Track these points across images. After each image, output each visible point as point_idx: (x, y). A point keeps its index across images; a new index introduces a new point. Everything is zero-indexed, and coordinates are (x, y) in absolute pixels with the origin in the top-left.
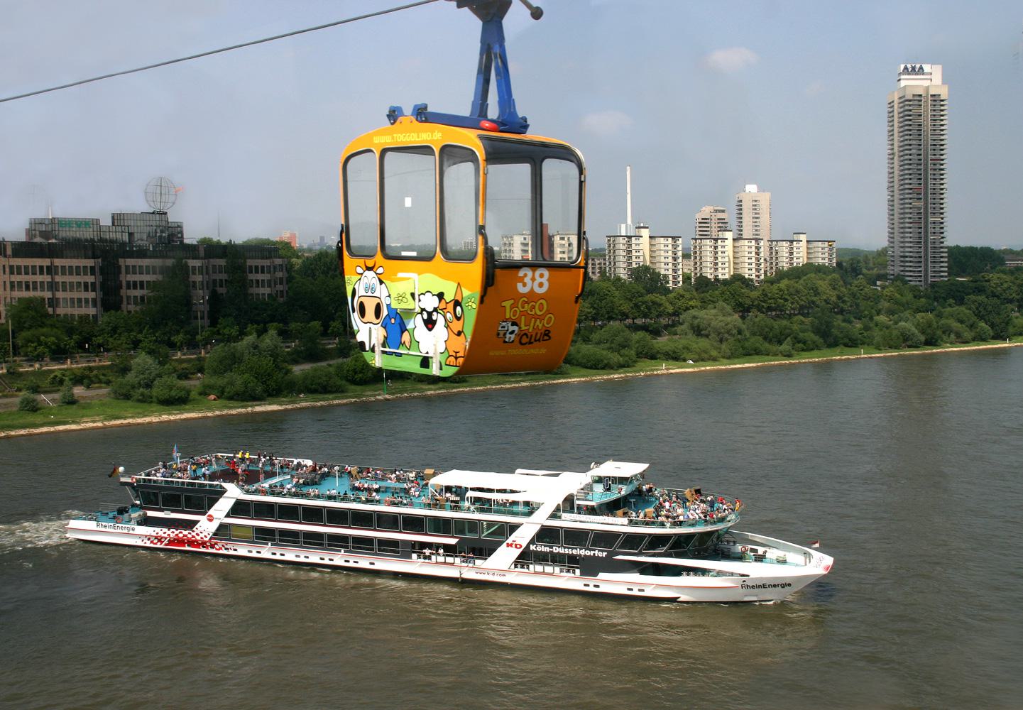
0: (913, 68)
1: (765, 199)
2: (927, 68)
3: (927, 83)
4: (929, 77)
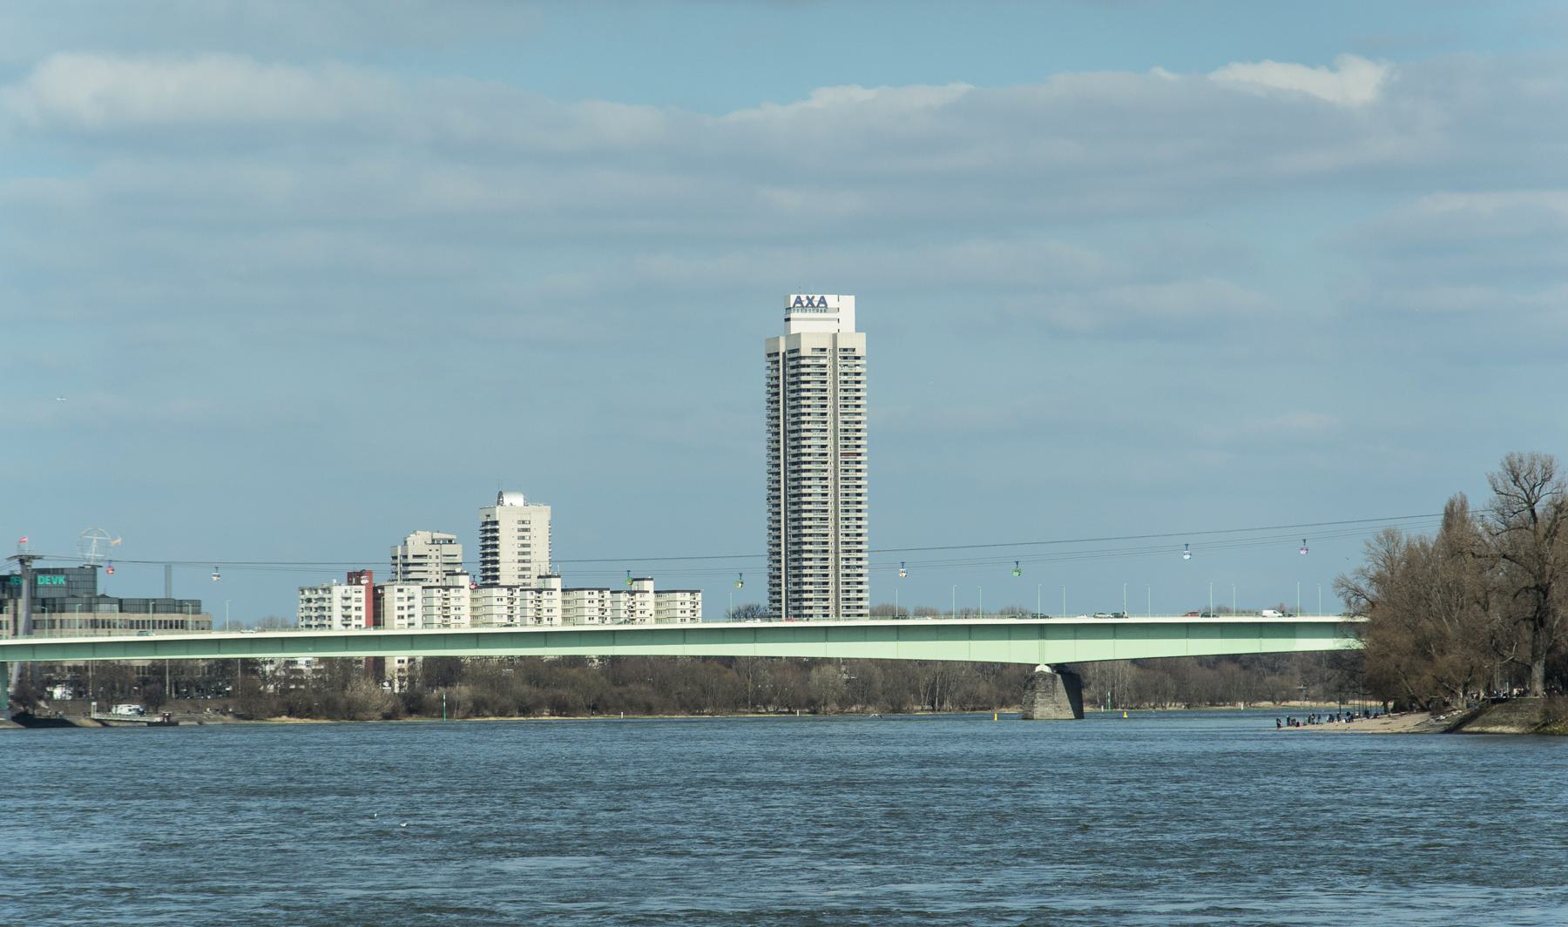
0: (810, 301)
1: (540, 518)
2: (831, 300)
3: (832, 328)
4: (836, 315)
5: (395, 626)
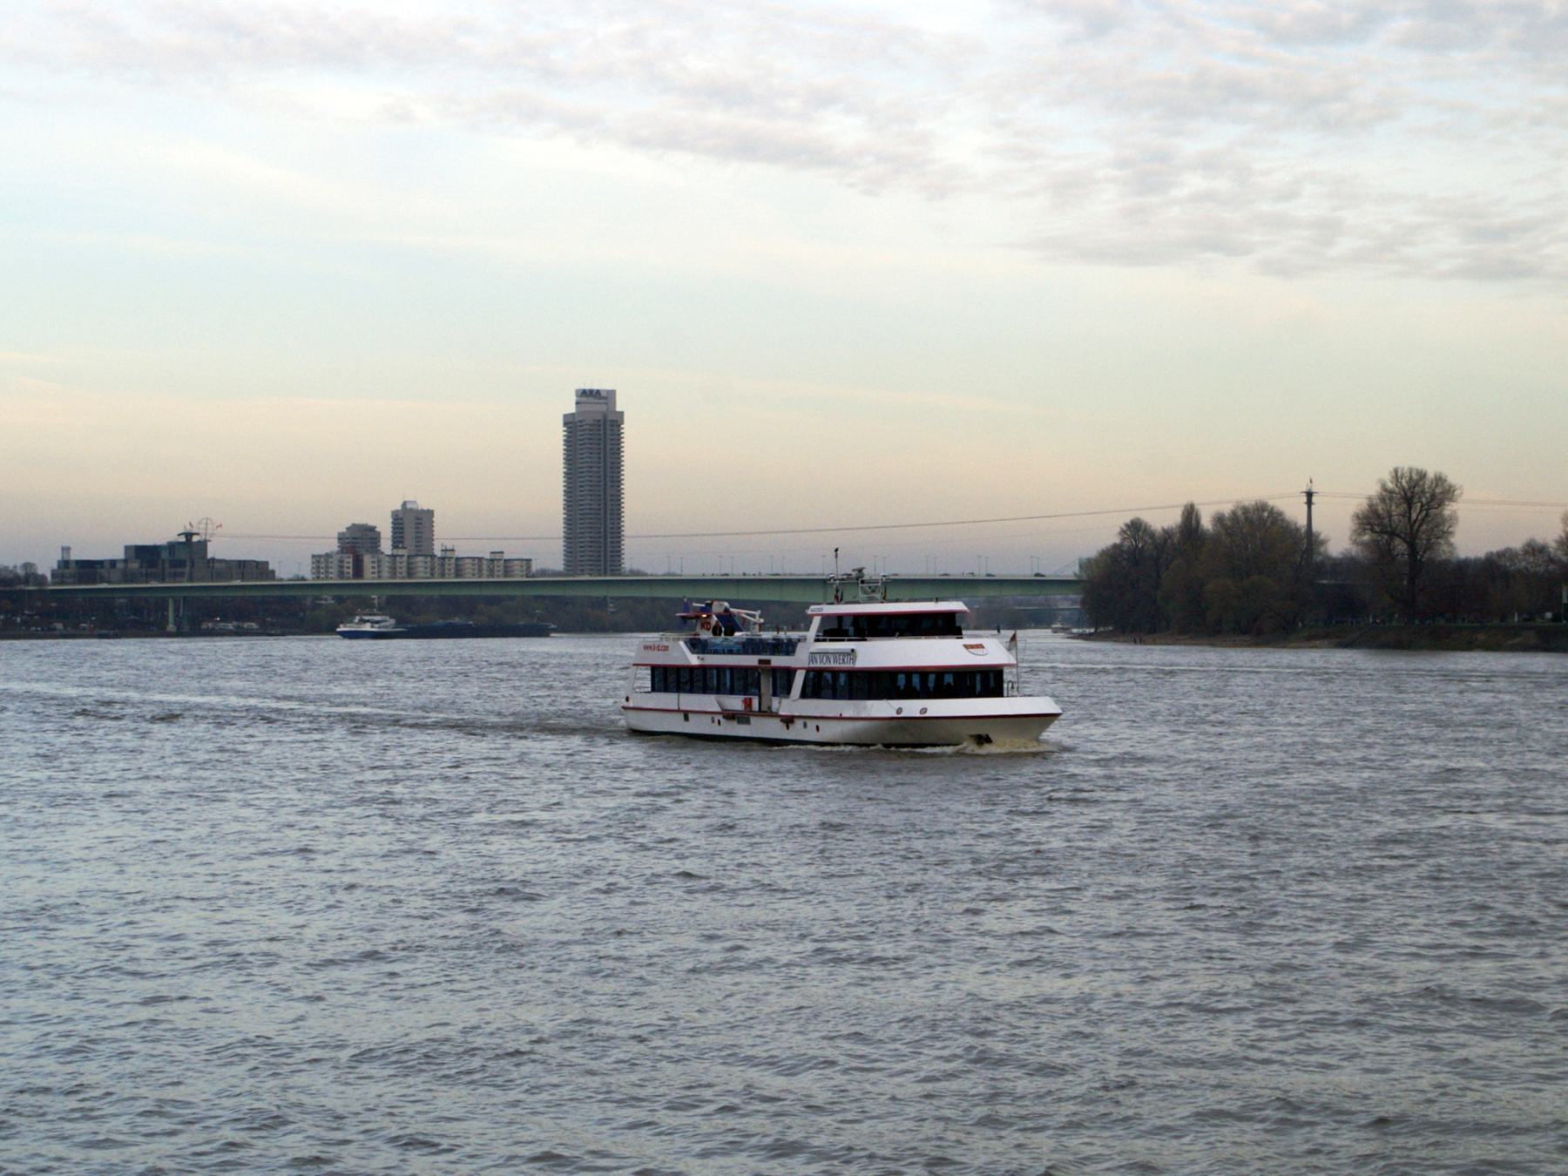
5: (369, 577)
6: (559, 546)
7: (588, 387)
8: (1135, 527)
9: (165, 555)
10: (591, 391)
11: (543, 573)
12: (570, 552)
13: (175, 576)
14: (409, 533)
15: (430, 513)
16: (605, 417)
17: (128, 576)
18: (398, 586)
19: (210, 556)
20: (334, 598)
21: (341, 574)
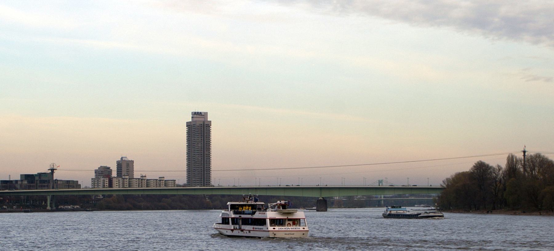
5: (115, 187)
6: (185, 174)
7: (196, 111)
8: (125, 166)
9: (37, 178)
10: (198, 113)
11: (86, 187)
12: (189, 177)
13: (42, 187)
14: (124, 169)
15: (132, 162)
16: (204, 122)
17: (22, 187)
18: (118, 192)
19: (54, 179)
20: (102, 195)
21: (104, 186)
